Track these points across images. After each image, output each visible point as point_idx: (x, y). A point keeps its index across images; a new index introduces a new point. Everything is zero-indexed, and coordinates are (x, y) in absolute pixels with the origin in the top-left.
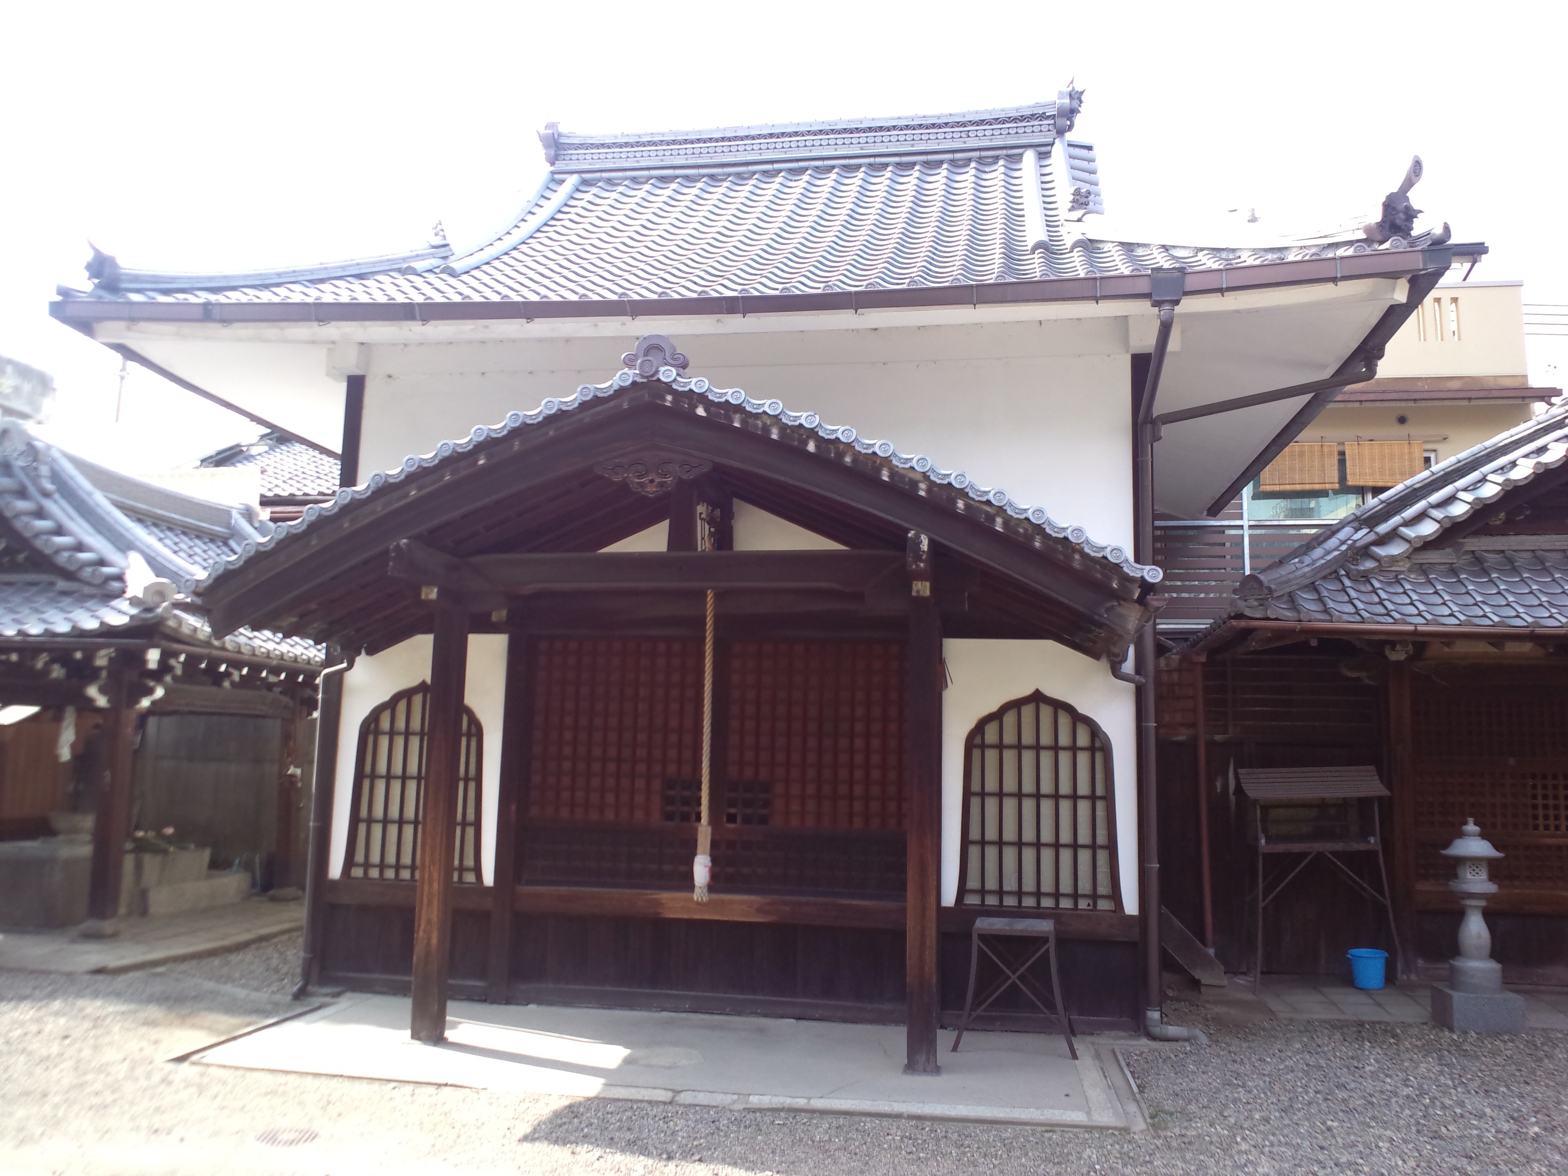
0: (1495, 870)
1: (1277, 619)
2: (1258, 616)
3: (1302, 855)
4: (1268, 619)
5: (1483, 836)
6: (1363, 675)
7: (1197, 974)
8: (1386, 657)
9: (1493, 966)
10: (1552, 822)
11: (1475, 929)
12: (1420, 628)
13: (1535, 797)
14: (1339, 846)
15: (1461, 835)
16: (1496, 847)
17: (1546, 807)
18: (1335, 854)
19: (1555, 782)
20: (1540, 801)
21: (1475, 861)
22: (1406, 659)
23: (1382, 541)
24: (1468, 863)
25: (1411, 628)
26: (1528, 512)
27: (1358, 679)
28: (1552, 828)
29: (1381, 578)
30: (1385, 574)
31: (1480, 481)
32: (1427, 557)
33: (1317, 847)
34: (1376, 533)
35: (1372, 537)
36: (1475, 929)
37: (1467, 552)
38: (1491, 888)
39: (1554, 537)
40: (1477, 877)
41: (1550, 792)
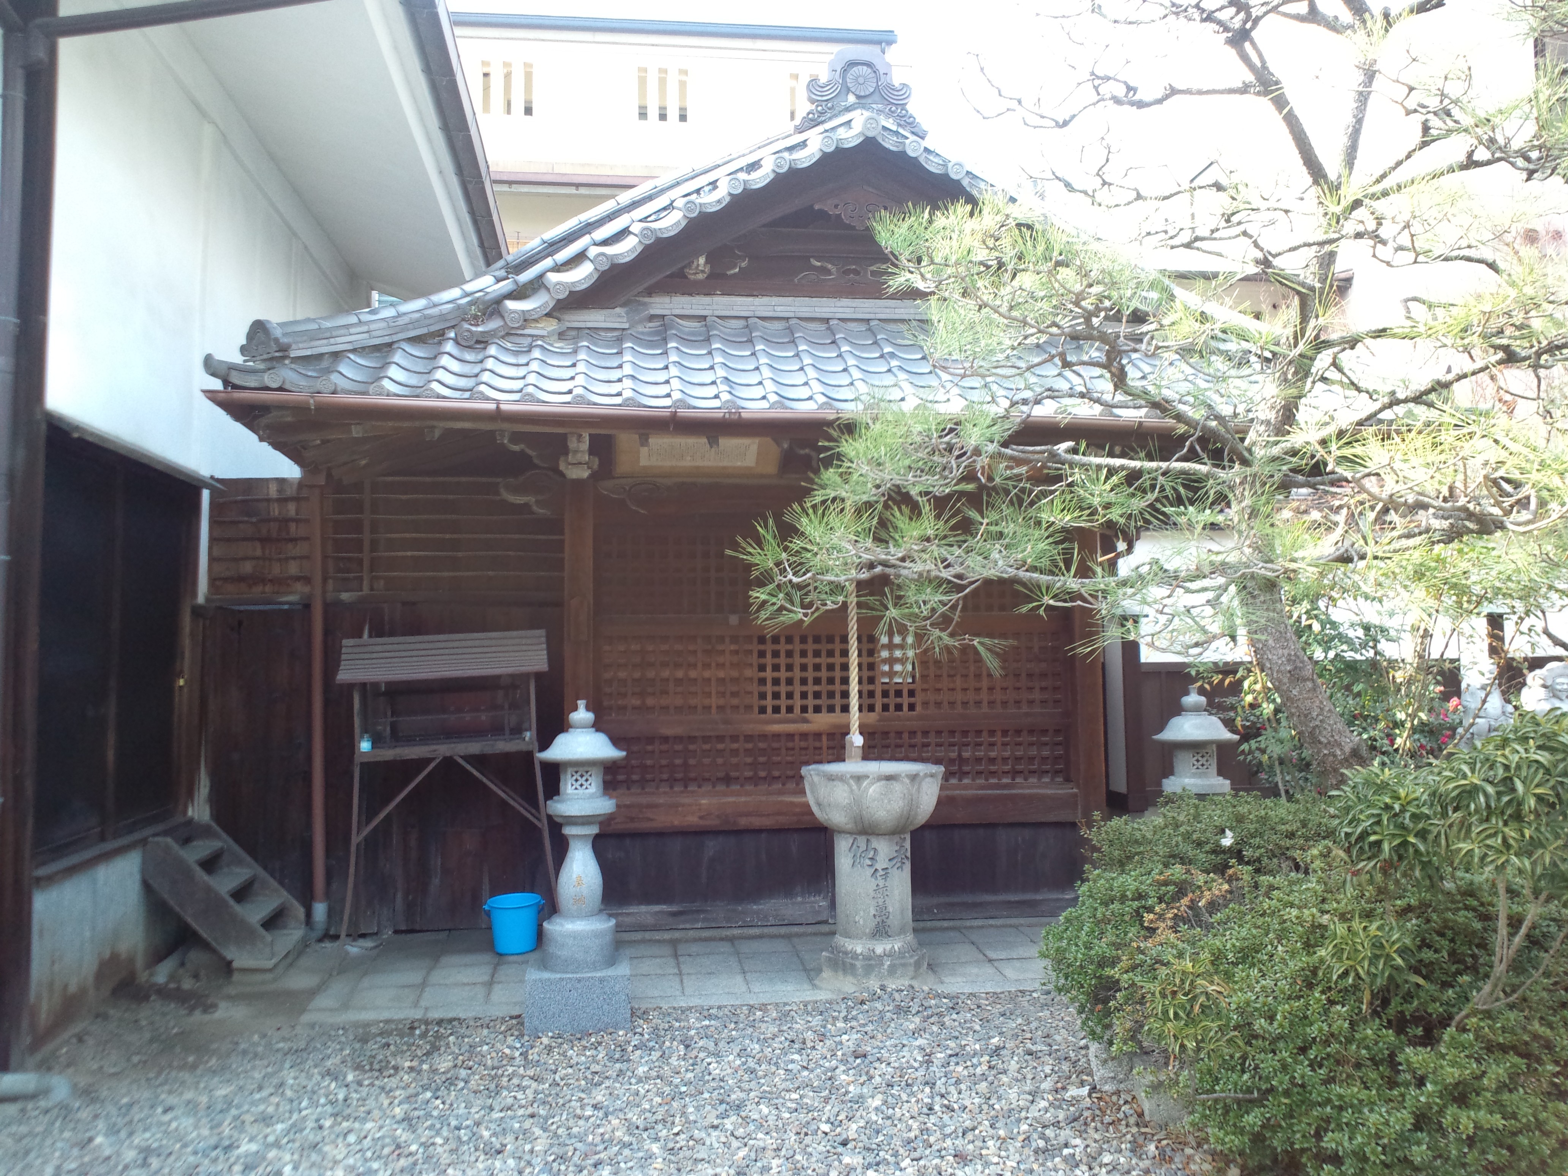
0: (612, 776)
1: (280, 389)
2: (253, 384)
3: (423, 763)
4: (267, 388)
5: (598, 726)
6: (530, 499)
7: (230, 953)
8: (562, 475)
9: (603, 925)
10: (783, 703)
11: (581, 871)
12: (503, 407)
13: (762, 668)
14: (474, 747)
15: (1178, 710)
16: (616, 741)
17: (776, 682)
18: (468, 758)
19: (789, 647)
20: (769, 674)
21: (582, 766)
22: (591, 476)
23: (519, 294)
24: (570, 771)
25: (492, 406)
26: (743, 265)
27: (526, 505)
28: (783, 710)
29: (509, 345)
30: (512, 338)
31: (665, 209)
32: (582, 318)
33: (442, 750)
34: (516, 282)
35: (506, 286)
36: (581, 871)
37: (652, 318)
38: (604, 806)
39: (775, 300)
40: (581, 791)
41: (782, 661)
